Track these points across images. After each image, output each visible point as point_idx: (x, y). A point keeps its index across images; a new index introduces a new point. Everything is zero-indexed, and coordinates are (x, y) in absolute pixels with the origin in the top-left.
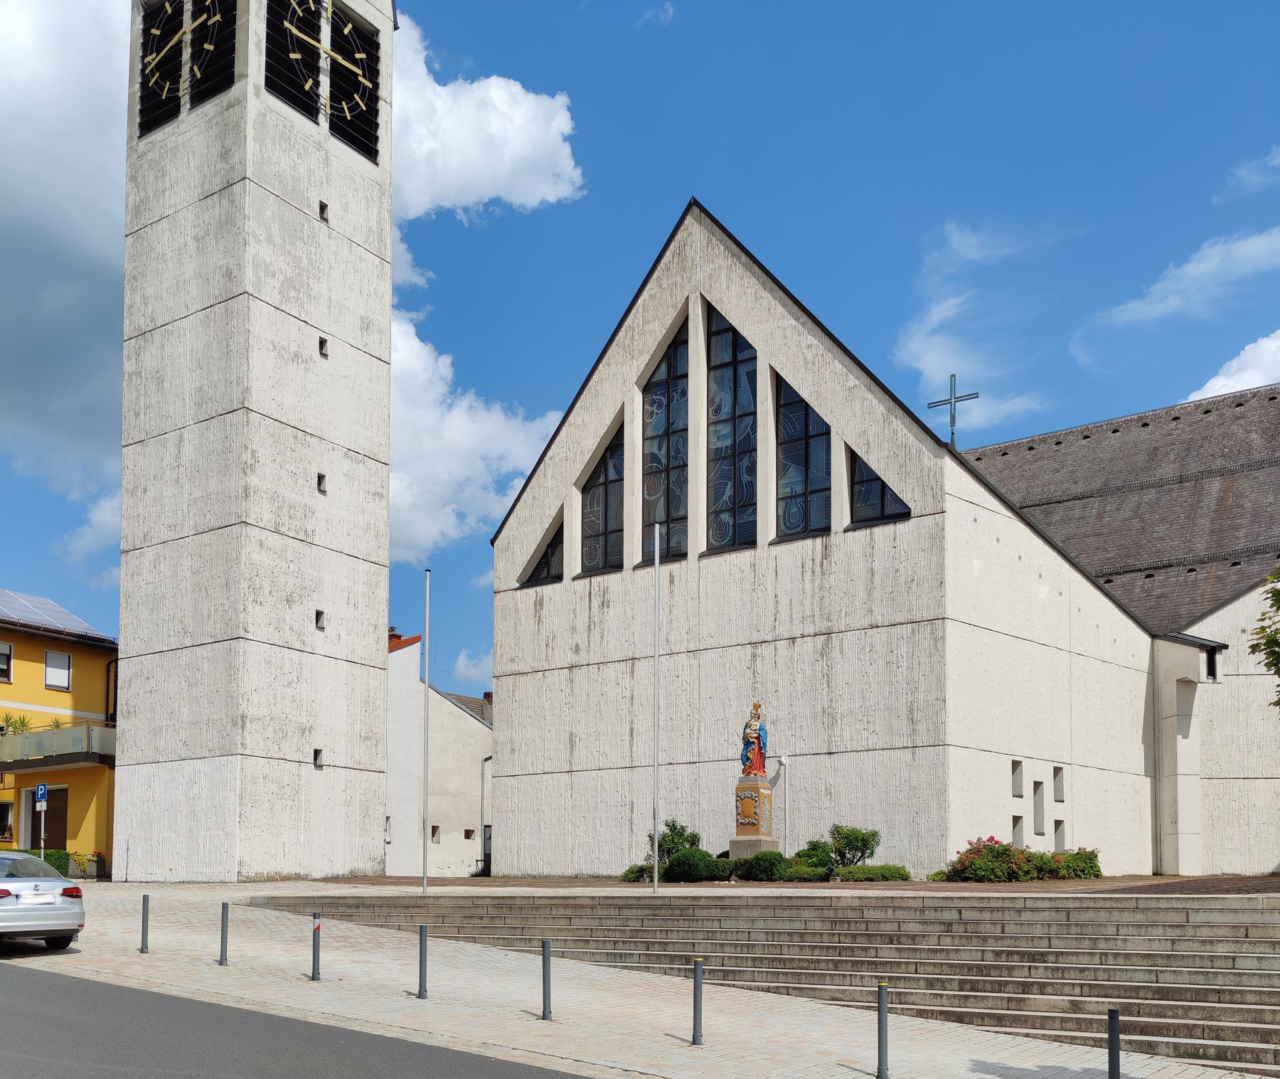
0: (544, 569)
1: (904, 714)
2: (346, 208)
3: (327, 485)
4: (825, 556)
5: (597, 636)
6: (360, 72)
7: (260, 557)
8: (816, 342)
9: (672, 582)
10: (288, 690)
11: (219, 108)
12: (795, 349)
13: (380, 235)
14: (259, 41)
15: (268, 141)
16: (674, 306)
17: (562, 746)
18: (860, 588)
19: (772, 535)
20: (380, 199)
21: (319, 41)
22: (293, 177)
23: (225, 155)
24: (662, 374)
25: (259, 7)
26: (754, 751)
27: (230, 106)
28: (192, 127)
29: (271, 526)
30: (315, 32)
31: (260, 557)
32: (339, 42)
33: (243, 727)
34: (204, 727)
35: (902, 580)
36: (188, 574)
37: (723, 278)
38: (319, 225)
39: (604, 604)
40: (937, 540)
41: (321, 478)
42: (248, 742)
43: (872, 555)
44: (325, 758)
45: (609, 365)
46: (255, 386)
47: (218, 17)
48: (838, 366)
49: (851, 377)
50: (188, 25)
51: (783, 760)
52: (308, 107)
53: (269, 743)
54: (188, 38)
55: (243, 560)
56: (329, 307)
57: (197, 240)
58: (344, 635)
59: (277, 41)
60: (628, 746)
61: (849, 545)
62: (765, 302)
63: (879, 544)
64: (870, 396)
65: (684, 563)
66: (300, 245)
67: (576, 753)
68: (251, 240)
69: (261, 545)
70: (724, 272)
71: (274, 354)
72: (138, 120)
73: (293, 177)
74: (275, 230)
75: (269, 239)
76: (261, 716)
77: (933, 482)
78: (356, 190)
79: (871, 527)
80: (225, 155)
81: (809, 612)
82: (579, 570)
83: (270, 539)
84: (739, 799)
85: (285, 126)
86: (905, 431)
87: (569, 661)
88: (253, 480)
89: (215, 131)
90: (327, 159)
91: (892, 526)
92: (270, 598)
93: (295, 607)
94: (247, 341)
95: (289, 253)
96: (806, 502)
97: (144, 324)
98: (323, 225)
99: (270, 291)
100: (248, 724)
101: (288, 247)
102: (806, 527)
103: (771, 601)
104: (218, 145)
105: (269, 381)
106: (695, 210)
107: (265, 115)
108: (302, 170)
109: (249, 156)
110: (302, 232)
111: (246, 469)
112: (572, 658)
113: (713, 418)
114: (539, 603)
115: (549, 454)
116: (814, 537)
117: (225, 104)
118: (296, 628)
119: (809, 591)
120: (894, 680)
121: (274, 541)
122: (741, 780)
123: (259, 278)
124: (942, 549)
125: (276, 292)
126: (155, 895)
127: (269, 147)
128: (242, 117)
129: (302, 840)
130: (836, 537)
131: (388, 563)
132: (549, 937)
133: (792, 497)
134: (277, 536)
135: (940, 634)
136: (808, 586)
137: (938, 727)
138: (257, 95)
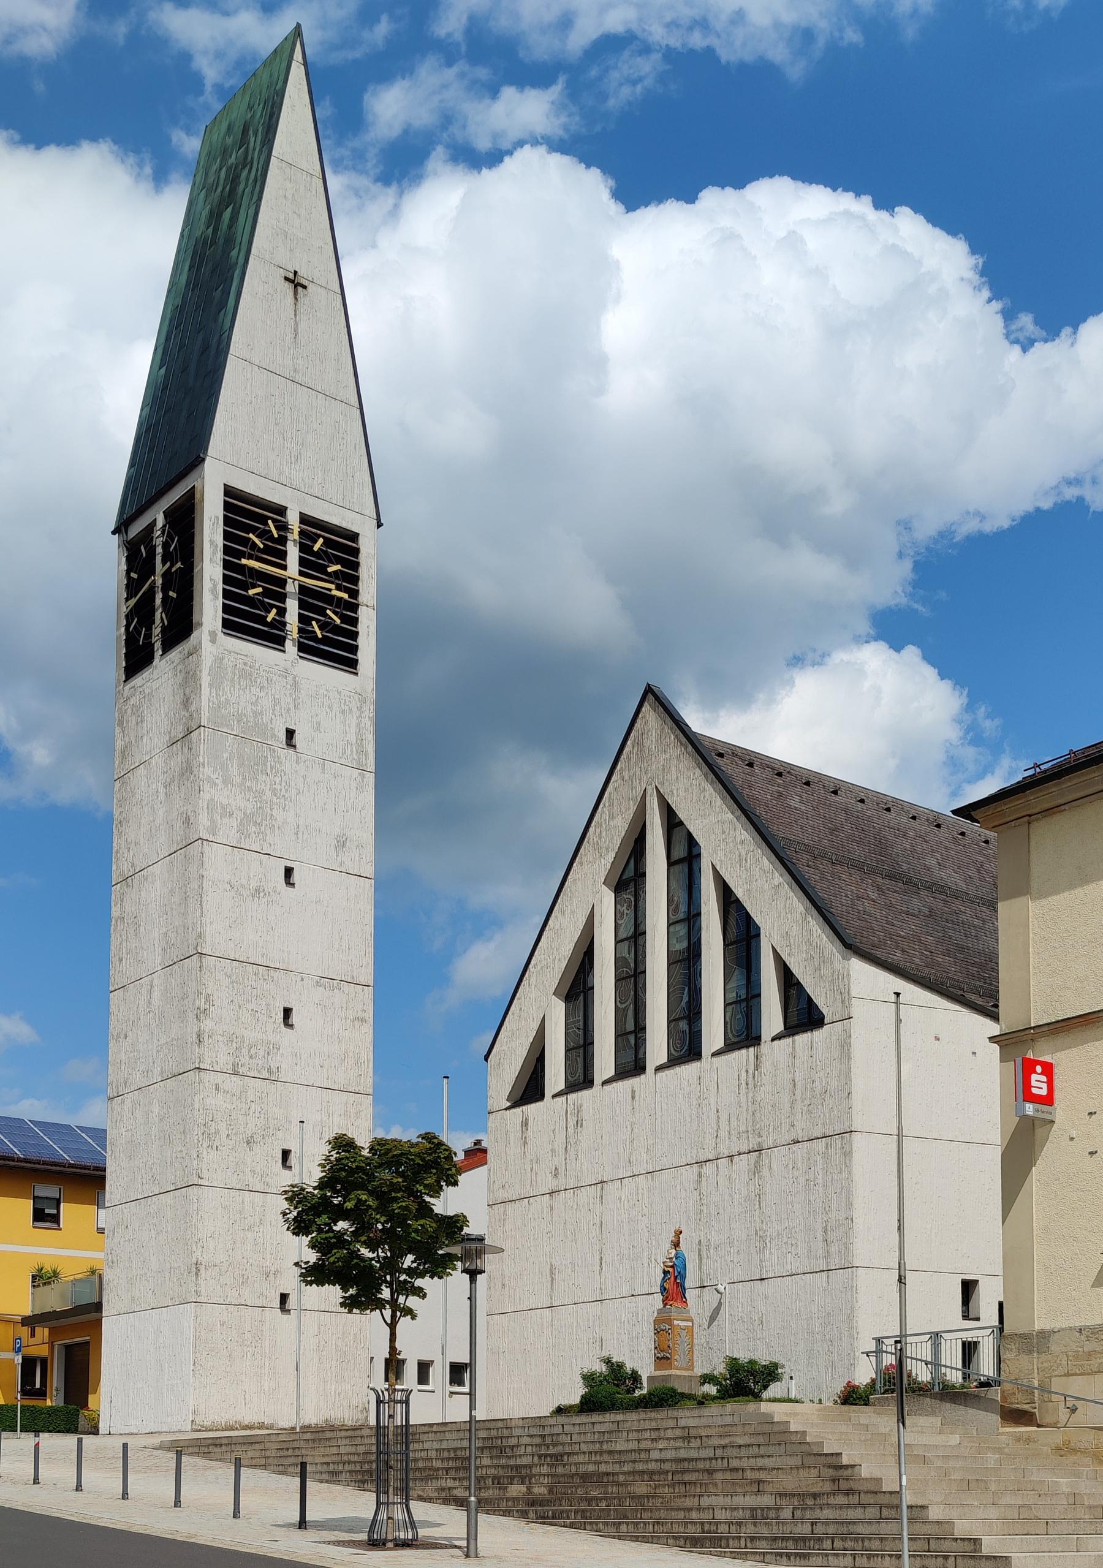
0: (530, 1088)
3: (295, 1018)
5: (573, 1157)
7: (214, 1101)
8: (748, 837)
9: (633, 1097)
10: (249, 1234)
11: (181, 656)
13: (360, 745)
16: (634, 799)
17: (544, 1280)
18: (785, 1098)
19: (719, 1043)
20: (360, 708)
21: (284, 568)
22: (254, 713)
23: (186, 703)
24: (630, 872)
25: (214, 553)
26: (673, 1285)
27: (190, 654)
28: (163, 670)
29: (229, 1068)
31: (214, 1101)
32: (309, 564)
33: (197, 1274)
34: (167, 1274)
36: (157, 1119)
37: (673, 769)
39: (578, 1123)
40: (845, 1046)
41: (287, 1012)
42: (203, 1289)
45: (581, 864)
46: (208, 931)
47: (179, 565)
49: (777, 874)
50: (160, 568)
51: (721, 1288)
52: (274, 638)
54: (159, 581)
55: (196, 1106)
57: (166, 787)
59: (236, 578)
61: (780, 1054)
62: (707, 794)
63: (799, 1053)
65: (643, 1076)
66: (262, 778)
67: (555, 1286)
68: (206, 787)
69: (217, 1089)
72: (124, 664)
73: (254, 713)
74: (234, 770)
79: (793, 1035)
80: (186, 703)
81: (743, 1128)
82: (562, 1086)
84: (657, 1332)
88: (208, 1025)
89: (180, 678)
90: (295, 684)
91: (809, 1034)
93: (257, 1149)
94: (201, 887)
96: (747, 1006)
97: (126, 868)
98: (291, 751)
99: (228, 831)
103: (714, 1116)
104: (181, 692)
105: (223, 925)
106: (650, 697)
107: (222, 659)
108: (266, 703)
109: (204, 704)
111: (201, 1014)
112: (552, 1184)
113: (673, 918)
114: (525, 1124)
115: (533, 962)
116: (748, 1047)
117: (186, 652)
118: (258, 1170)
119: (744, 1105)
121: (232, 1083)
122: (659, 1311)
123: (214, 822)
124: (849, 1059)
126: (132, 1442)
127: (227, 689)
128: (198, 665)
130: (766, 1046)
131: (371, 1091)
132: (308, 1460)
133: (737, 1002)
134: (234, 1078)
136: (743, 1099)
138: (213, 641)
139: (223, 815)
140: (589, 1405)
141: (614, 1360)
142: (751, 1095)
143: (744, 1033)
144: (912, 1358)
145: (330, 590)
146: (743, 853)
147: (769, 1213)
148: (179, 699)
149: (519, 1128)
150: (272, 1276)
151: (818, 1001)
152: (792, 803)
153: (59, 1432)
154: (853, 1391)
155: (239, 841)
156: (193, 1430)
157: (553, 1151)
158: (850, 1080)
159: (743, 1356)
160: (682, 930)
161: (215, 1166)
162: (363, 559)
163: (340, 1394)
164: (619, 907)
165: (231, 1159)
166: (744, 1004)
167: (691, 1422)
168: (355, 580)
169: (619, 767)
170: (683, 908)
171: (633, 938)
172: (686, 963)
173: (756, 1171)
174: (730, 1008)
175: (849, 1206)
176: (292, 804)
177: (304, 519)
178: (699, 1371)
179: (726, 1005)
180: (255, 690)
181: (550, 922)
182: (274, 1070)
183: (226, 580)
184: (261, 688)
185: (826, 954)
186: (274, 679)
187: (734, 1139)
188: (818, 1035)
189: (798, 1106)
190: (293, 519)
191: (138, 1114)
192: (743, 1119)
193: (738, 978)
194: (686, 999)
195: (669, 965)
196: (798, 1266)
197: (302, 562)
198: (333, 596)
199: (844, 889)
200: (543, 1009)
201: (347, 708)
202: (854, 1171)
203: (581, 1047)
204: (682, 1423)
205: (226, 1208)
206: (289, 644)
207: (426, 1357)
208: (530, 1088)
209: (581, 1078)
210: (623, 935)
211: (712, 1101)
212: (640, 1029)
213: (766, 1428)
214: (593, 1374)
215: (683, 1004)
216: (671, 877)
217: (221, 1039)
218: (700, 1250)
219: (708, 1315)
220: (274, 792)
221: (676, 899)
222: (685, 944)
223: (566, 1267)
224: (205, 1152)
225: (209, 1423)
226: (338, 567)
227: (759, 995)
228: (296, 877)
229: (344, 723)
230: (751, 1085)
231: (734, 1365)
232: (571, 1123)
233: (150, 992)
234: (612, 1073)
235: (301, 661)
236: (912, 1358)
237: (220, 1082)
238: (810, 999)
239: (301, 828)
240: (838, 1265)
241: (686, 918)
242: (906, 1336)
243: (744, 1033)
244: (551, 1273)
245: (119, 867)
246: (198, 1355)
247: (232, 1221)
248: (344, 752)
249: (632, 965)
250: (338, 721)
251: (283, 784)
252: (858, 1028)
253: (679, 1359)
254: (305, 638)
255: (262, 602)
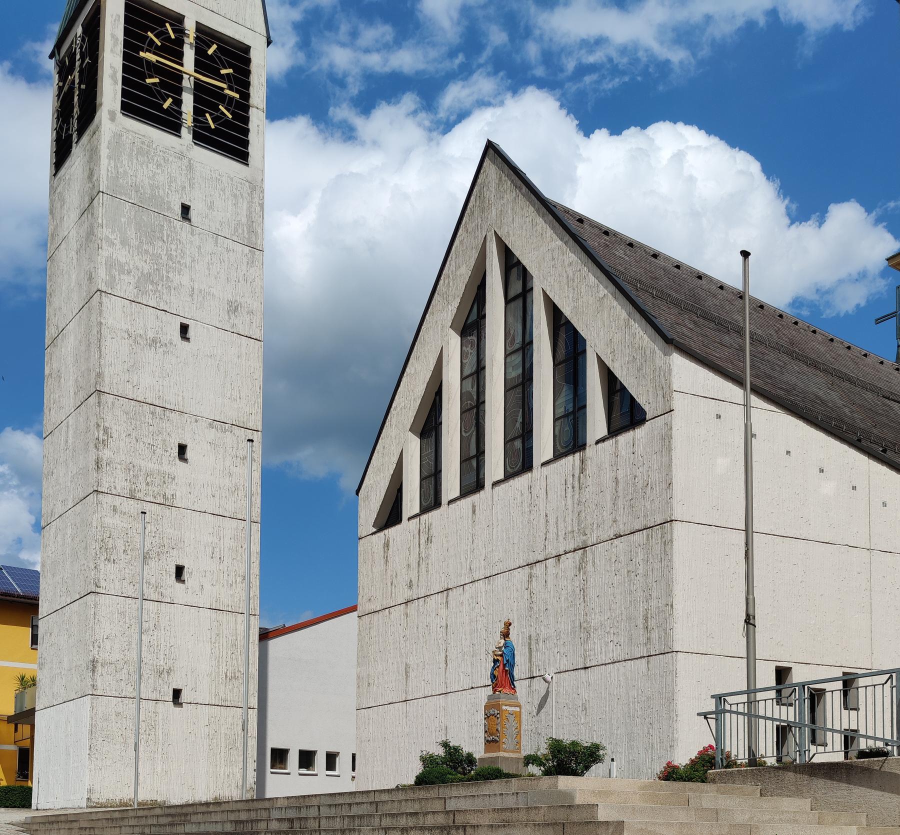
0: (391, 515)
1: (640, 622)
2: (211, 207)
3: (189, 454)
4: (582, 470)
6: (224, 86)
8: (576, 258)
9: (474, 512)
12: (560, 269)
14: (115, 73)
15: (124, 158)
18: (608, 497)
21: (182, 65)
22: (151, 186)
24: (474, 316)
25: (115, 45)
26: (503, 673)
29: (126, 493)
30: (178, 56)
32: (203, 64)
33: (93, 671)
35: (639, 486)
37: (510, 212)
38: (180, 224)
39: (429, 540)
40: (666, 439)
42: (99, 685)
43: (616, 464)
44: (184, 698)
45: (433, 313)
46: (107, 371)
48: (591, 277)
49: (601, 287)
51: (549, 678)
52: (172, 125)
53: (123, 684)
55: (95, 524)
56: (191, 296)
58: (207, 586)
59: (133, 68)
60: (443, 673)
62: (538, 228)
64: (615, 303)
65: (482, 492)
67: (409, 683)
68: (105, 245)
70: (510, 206)
71: (131, 341)
73: (151, 186)
74: (131, 233)
75: (124, 242)
76: (113, 660)
77: (663, 381)
78: (223, 190)
79: (616, 435)
81: (570, 529)
83: (125, 504)
84: (487, 717)
85: (143, 143)
86: (642, 333)
87: (405, 596)
88: (106, 454)
90: (190, 167)
92: (123, 556)
93: (152, 563)
94: (100, 332)
95: (147, 252)
98: (186, 224)
99: (126, 286)
100: (99, 668)
101: (145, 247)
102: (574, 445)
103: (542, 520)
106: (491, 151)
107: (121, 135)
108: (162, 179)
110: (161, 231)
111: (99, 444)
112: (407, 594)
113: (510, 349)
114: (387, 545)
116: (574, 453)
120: (633, 589)
124: (670, 449)
125: (132, 287)
127: (125, 162)
129: (159, 769)
130: (590, 451)
134: (131, 502)
135: (667, 537)
136: (569, 502)
137: (667, 632)
138: (113, 118)
139: (121, 272)
140: (421, 781)
141: (451, 745)
142: (577, 497)
143: (571, 440)
144: (766, 718)
145: (222, 89)
146: (571, 274)
147: (593, 606)
148: (86, 174)
149: (382, 546)
150: (165, 674)
151: (641, 400)
152: (617, 253)
153: (15, 807)
154: (673, 772)
155: (137, 296)
156: (88, 807)
157: (409, 566)
158: (671, 471)
159: (566, 737)
160: (517, 358)
161: (112, 577)
162: (253, 67)
163: (228, 776)
164: (464, 348)
165: (127, 571)
166: (571, 417)
167: (462, 805)
168: (247, 85)
169: (464, 222)
170: (519, 339)
171: (475, 375)
172: (520, 388)
173: (581, 568)
174: (558, 423)
175: (670, 593)
176: (187, 270)
177: (200, 28)
178: (524, 753)
179: (555, 420)
180: (152, 166)
181: (408, 369)
182: (170, 497)
183: (125, 69)
184: (159, 166)
185: (648, 352)
186: (171, 159)
187: (561, 538)
188: (640, 433)
189: (620, 502)
190: (190, 27)
191: (59, 538)
192: (569, 520)
193: (566, 393)
194: (520, 420)
195: (506, 391)
196: (618, 654)
197: (198, 64)
198: (225, 96)
199: (666, 317)
200: (401, 443)
201: (238, 193)
202: (675, 559)
203: (432, 477)
204: (452, 805)
205: (122, 613)
206: (184, 131)
207: (333, 749)
208: (391, 515)
209: (432, 500)
210: (467, 372)
211: (542, 507)
212: (480, 453)
213: (561, 815)
214: (431, 756)
215: (518, 425)
216: (508, 313)
217: (119, 467)
218: (530, 644)
219: (537, 703)
220: (170, 257)
221: (512, 332)
222: (520, 371)
223: (418, 665)
224: (102, 564)
225: (104, 801)
226: (230, 71)
227: (585, 406)
228: (191, 333)
229: (236, 205)
230: (577, 488)
231: (557, 747)
232: (423, 541)
233: (67, 432)
234: (458, 494)
235: (196, 147)
236: (766, 718)
237: (118, 504)
238: (632, 399)
239: (196, 291)
240: (656, 648)
241: (521, 349)
242: (756, 691)
243: (571, 440)
244: (407, 672)
245: (50, 332)
246: (94, 741)
247: (128, 625)
248: (236, 230)
249: (475, 397)
250: (230, 202)
251: (179, 251)
252: (678, 421)
253: (507, 742)
254: (200, 128)
255: (159, 92)
